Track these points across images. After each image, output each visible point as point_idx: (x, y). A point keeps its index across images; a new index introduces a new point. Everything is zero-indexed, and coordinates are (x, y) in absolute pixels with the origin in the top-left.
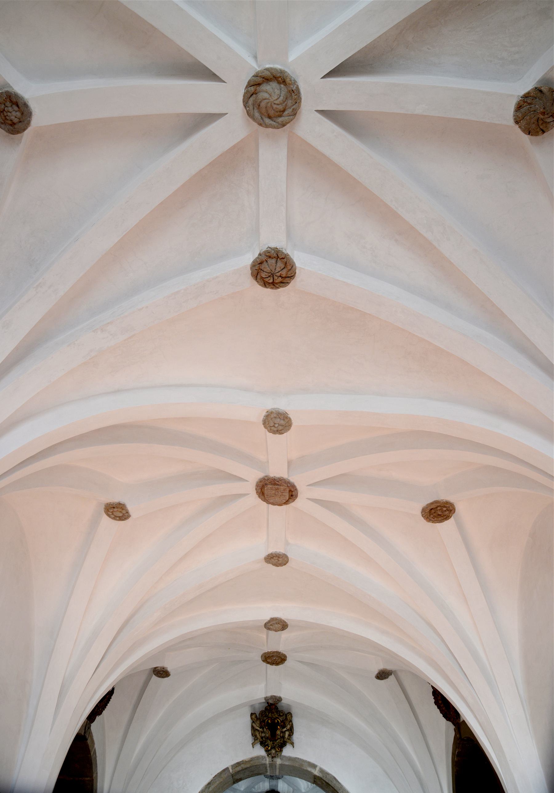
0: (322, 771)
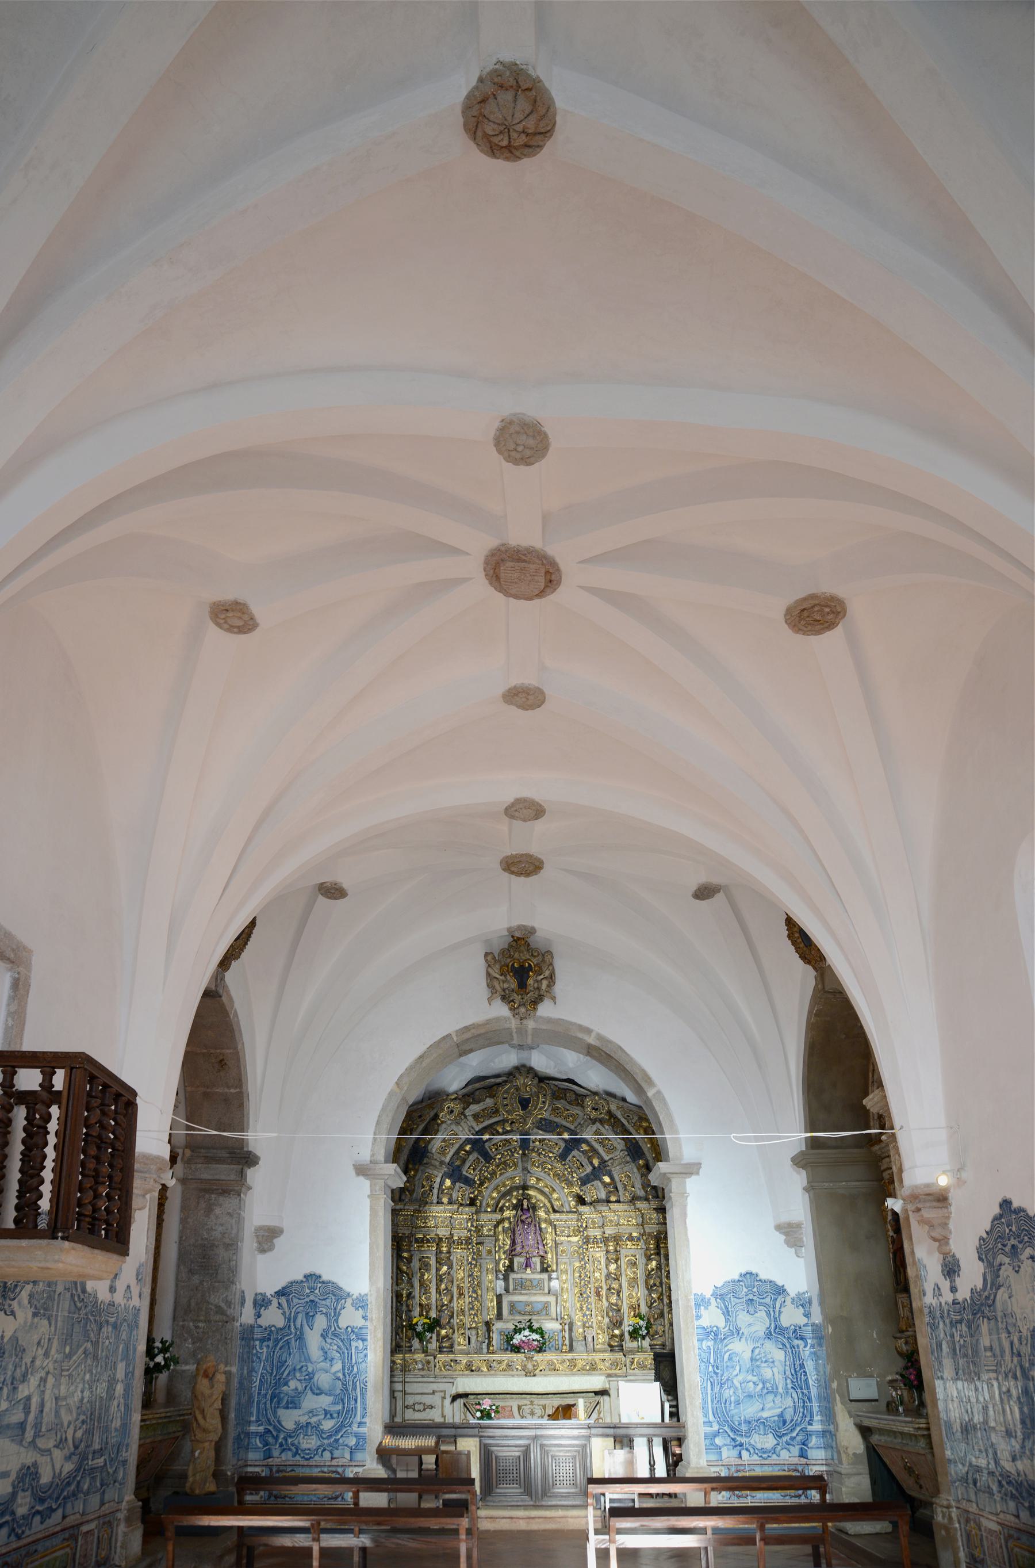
0: (600, 1037)
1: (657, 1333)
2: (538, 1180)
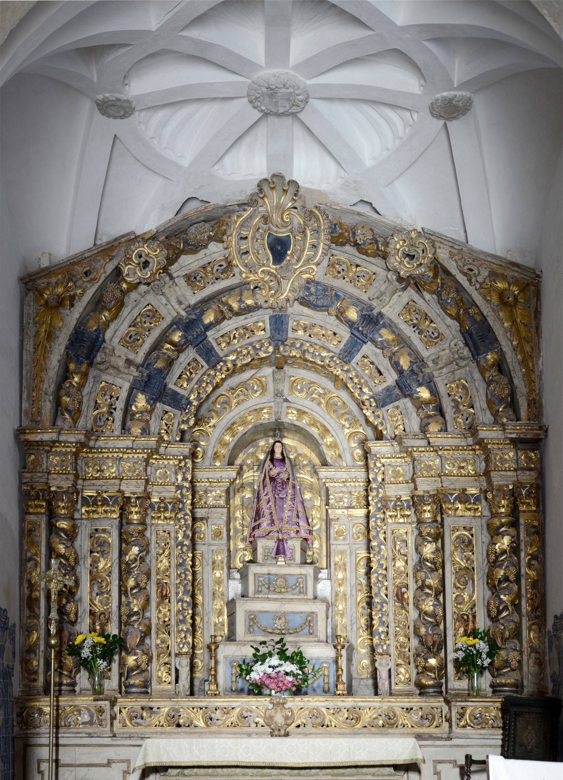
1: (506, 664)
2: (301, 413)
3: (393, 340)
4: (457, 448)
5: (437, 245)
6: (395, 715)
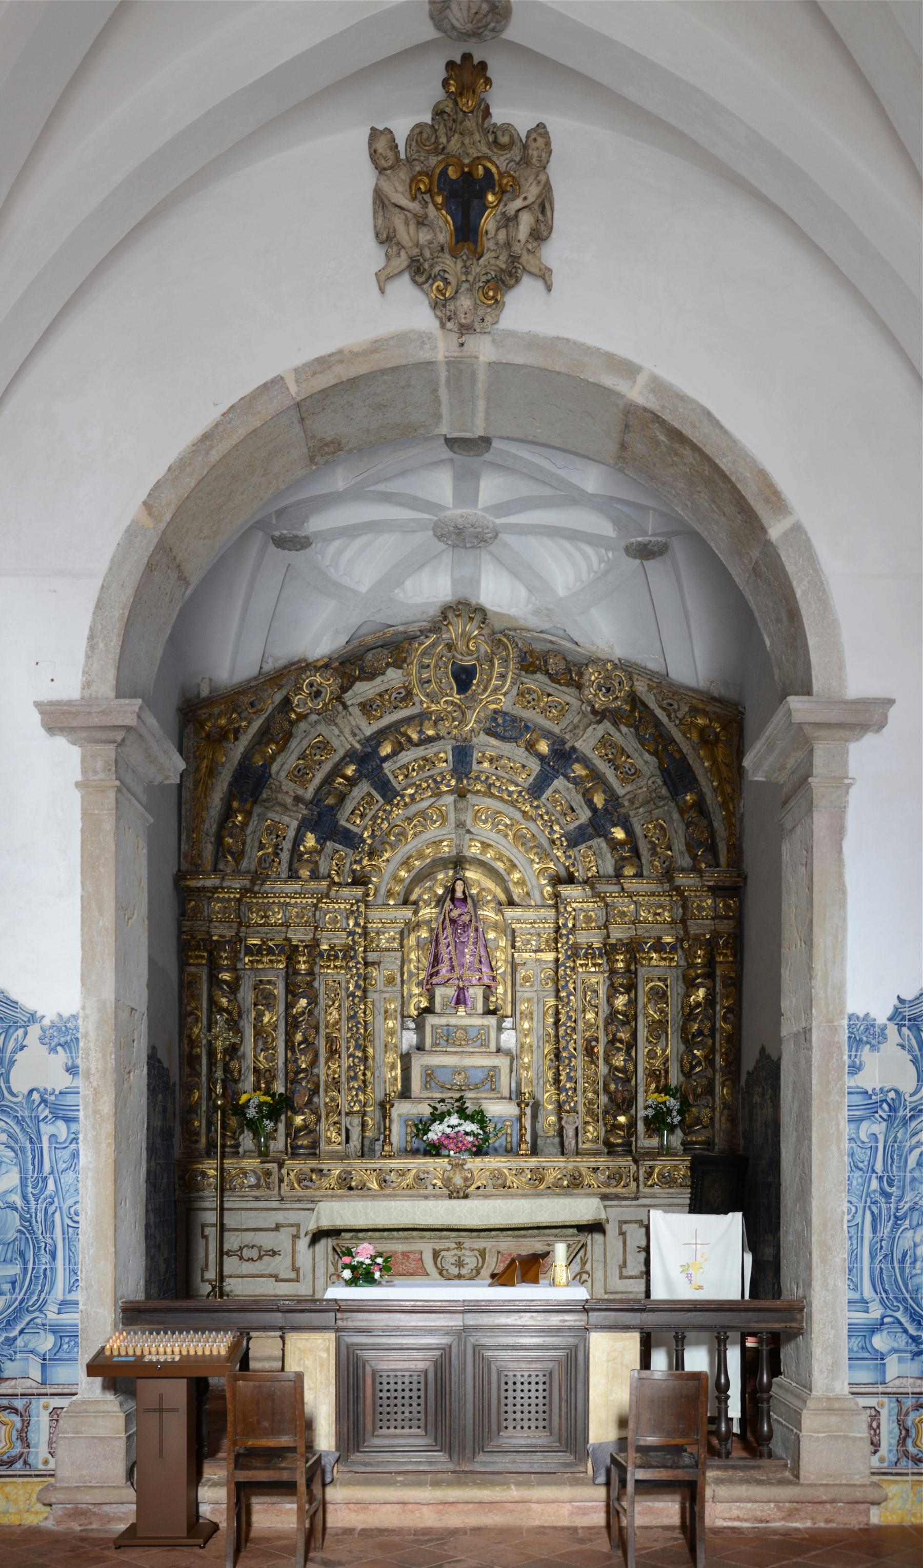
0: (658, 386)
1: (698, 1121)
2: (486, 846)
3: (587, 776)
4: (653, 894)
5: (635, 677)
6: (581, 1175)
